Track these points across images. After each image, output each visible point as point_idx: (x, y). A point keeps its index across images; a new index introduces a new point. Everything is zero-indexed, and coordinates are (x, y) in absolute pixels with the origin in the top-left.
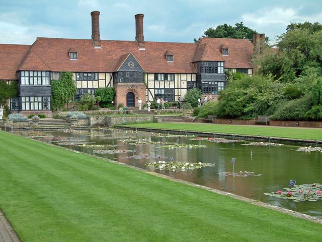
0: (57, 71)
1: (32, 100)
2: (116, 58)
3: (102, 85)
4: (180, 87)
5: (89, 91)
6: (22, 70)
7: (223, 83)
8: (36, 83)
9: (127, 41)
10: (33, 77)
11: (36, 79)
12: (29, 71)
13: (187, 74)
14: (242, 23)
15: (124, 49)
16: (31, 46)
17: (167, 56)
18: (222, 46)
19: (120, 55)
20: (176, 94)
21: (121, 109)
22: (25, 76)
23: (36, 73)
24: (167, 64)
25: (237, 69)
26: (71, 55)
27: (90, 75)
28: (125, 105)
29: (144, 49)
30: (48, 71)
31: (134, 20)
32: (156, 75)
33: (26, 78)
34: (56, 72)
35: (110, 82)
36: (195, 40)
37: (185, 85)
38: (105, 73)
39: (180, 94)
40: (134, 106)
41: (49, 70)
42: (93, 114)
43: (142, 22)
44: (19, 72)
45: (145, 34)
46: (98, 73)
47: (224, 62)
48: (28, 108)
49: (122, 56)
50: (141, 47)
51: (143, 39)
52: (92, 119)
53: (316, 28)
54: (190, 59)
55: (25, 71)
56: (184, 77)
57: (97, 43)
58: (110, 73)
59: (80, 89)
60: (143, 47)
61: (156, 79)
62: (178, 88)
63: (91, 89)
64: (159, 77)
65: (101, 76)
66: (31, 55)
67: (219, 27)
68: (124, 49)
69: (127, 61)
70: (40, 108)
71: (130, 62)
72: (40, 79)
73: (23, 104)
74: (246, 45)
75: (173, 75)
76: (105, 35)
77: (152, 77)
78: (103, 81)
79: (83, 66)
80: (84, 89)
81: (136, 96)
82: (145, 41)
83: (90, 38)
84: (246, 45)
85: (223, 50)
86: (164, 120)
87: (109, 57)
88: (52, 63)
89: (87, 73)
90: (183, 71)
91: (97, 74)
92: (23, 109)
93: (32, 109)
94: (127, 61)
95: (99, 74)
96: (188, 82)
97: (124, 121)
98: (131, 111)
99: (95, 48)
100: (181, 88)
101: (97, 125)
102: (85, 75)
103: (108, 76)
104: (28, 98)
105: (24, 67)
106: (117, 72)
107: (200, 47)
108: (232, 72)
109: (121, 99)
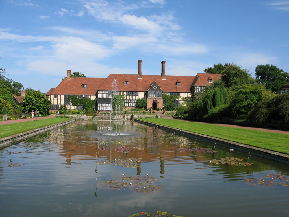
0: (128, 91)
1: (103, 92)
2: (149, 84)
8: (105, 97)
9: (156, 75)
10: (104, 94)
11: (105, 95)
13: (187, 93)
16: (106, 79)
22: (100, 93)
24: (176, 87)
26: (209, 81)
30: (101, 91)
31: (161, 64)
44: (98, 91)
45: (166, 71)
50: (163, 78)
54: (190, 85)
55: (100, 91)
58: (144, 92)
65: (140, 93)
68: (154, 79)
73: (99, 107)
81: (158, 104)
82: (166, 75)
89: (132, 92)
90: (186, 91)
91: (151, 92)
92: (99, 109)
93: (103, 109)
94: (153, 86)
95: (139, 92)
99: (139, 79)
102: (132, 92)
109: (150, 105)
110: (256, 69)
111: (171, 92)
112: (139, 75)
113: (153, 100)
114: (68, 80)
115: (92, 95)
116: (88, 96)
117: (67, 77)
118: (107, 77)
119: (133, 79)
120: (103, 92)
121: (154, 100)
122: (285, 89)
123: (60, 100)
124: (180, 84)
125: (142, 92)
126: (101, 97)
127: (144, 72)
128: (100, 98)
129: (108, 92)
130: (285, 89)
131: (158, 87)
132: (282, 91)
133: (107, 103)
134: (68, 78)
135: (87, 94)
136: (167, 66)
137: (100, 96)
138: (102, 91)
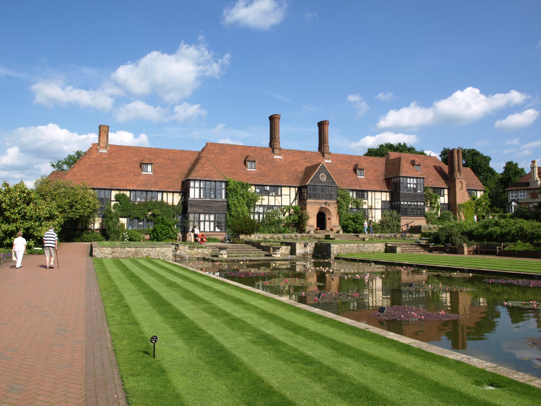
3: (286, 202)
10: (205, 221)
11: (207, 224)
13: (381, 192)
17: (142, 165)
22: (194, 187)
24: (358, 179)
26: (249, 164)
29: (281, 157)
35: (295, 199)
37: (379, 205)
39: (373, 216)
41: (225, 180)
50: (327, 159)
56: (378, 195)
58: (295, 187)
60: (329, 159)
65: (285, 191)
68: (308, 160)
69: (319, 172)
70: (212, 230)
75: (165, 194)
79: (263, 178)
81: (327, 217)
87: (292, 168)
94: (319, 172)
95: (283, 188)
99: (275, 157)
103: (293, 191)
106: (306, 187)
110: (402, 144)
111: (435, 188)
112: (276, 148)
113: (319, 207)
114: (100, 151)
115: (170, 192)
116: (160, 195)
117: (99, 144)
118: (199, 149)
119: (263, 158)
120: (197, 184)
121: (322, 208)
122: (518, 190)
123: (375, 209)
124: (253, 164)
125: (290, 187)
126: (197, 196)
127: (284, 143)
128: (195, 202)
129: (417, 181)
130: (518, 190)
131: (329, 176)
132: (512, 193)
133: (212, 214)
134: (101, 145)
135: (158, 190)
136: (283, 129)
137: (194, 194)
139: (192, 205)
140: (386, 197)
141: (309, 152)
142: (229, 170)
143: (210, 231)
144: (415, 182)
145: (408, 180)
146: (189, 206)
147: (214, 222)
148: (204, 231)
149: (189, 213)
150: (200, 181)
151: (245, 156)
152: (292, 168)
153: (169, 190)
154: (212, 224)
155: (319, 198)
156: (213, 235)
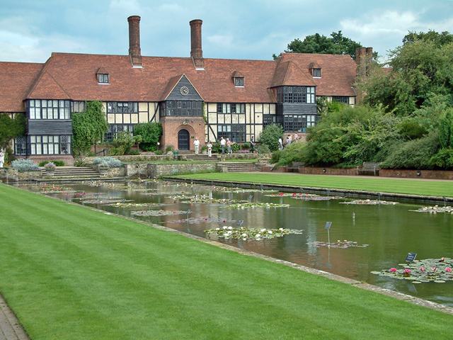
3: (144, 119)
4: (253, 122)
5: (125, 128)
6: (31, 98)
7: (313, 117)
8: (50, 117)
10: (47, 108)
11: (50, 110)
12: (41, 100)
14: (340, 32)
15: (174, 69)
16: (43, 65)
17: (235, 78)
18: (312, 64)
19: (169, 77)
20: (248, 132)
21: (170, 153)
22: (35, 107)
23: (50, 102)
24: (234, 90)
25: (333, 96)
26: (100, 77)
27: (127, 106)
28: (176, 148)
29: (203, 69)
31: (189, 28)
32: (220, 106)
33: (37, 109)
34: (79, 101)
35: (154, 116)
36: (274, 56)
37: (260, 120)
38: (148, 102)
40: (189, 149)
41: (69, 98)
42: (131, 161)
43: (200, 32)
45: (204, 48)
46: (138, 102)
47: (315, 87)
48: (39, 152)
49: (172, 78)
50: (198, 66)
51: (201, 55)
52: (129, 167)
53: (445, 39)
56: (259, 108)
57: (137, 60)
58: (154, 102)
59: (112, 125)
60: (201, 66)
61: (220, 111)
62: (250, 124)
63: (128, 125)
64: (224, 109)
65: (143, 107)
66: (44, 78)
67: (308, 38)
68: (174, 69)
69: (179, 86)
70: (57, 152)
71: (183, 87)
72: (56, 111)
73: (33, 146)
74: (346, 63)
75: (243, 106)
76: (147, 49)
77: (213, 108)
78: (145, 115)
79: (117, 93)
80: (118, 124)
81: (191, 135)
83: (127, 53)
84: (346, 63)
85: (313, 70)
86: (230, 168)
87: (153, 80)
88: (74, 89)
89: (123, 102)
90: (258, 100)
91: (136, 104)
92: (33, 153)
94: (179, 86)
95: (140, 104)
96: (264, 116)
97: (175, 170)
98: (184, 156)
99: (134, 67)
100: (255, 124)
101: (136, 176)
103: (152, 107)
104: (39, 138)
105: (34, 94)
106: (165, 102)
107: (281, 66)
108: (327, 101)
109: (171, 139)
125: (148, 102)
126: (56, 117)
129: (60, 139)
131: (193, 91)
138: (41, 100)
139: (33, 127)
140: (270, 110)
141: (178, 58)
142: (78, 86)
143: (54, 154)
144: (313, 120)
145: (308, 89)
146: (29, 127)
147: (59, 144)
148: (48, 154)
149: (30, 135)
150: (65, 100)
151: (97, 68)
152: (153, 80)
153: (124, 100)
154: (57, 146)
155: (180, 115)
156: (57, 158)
